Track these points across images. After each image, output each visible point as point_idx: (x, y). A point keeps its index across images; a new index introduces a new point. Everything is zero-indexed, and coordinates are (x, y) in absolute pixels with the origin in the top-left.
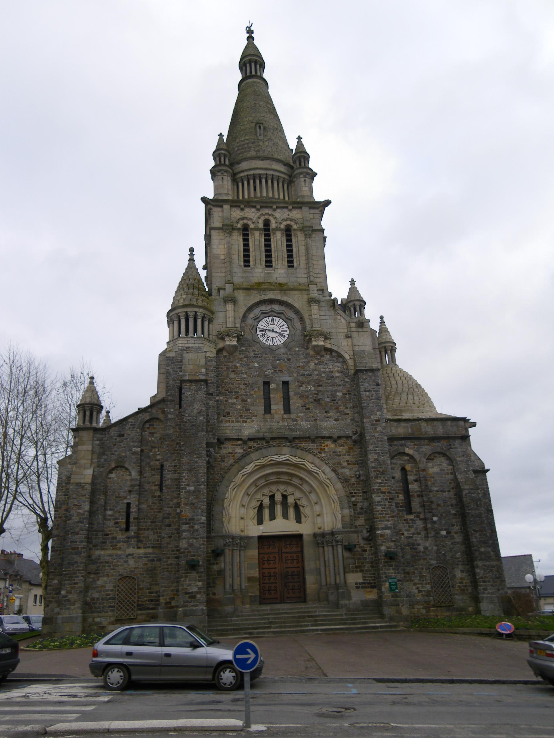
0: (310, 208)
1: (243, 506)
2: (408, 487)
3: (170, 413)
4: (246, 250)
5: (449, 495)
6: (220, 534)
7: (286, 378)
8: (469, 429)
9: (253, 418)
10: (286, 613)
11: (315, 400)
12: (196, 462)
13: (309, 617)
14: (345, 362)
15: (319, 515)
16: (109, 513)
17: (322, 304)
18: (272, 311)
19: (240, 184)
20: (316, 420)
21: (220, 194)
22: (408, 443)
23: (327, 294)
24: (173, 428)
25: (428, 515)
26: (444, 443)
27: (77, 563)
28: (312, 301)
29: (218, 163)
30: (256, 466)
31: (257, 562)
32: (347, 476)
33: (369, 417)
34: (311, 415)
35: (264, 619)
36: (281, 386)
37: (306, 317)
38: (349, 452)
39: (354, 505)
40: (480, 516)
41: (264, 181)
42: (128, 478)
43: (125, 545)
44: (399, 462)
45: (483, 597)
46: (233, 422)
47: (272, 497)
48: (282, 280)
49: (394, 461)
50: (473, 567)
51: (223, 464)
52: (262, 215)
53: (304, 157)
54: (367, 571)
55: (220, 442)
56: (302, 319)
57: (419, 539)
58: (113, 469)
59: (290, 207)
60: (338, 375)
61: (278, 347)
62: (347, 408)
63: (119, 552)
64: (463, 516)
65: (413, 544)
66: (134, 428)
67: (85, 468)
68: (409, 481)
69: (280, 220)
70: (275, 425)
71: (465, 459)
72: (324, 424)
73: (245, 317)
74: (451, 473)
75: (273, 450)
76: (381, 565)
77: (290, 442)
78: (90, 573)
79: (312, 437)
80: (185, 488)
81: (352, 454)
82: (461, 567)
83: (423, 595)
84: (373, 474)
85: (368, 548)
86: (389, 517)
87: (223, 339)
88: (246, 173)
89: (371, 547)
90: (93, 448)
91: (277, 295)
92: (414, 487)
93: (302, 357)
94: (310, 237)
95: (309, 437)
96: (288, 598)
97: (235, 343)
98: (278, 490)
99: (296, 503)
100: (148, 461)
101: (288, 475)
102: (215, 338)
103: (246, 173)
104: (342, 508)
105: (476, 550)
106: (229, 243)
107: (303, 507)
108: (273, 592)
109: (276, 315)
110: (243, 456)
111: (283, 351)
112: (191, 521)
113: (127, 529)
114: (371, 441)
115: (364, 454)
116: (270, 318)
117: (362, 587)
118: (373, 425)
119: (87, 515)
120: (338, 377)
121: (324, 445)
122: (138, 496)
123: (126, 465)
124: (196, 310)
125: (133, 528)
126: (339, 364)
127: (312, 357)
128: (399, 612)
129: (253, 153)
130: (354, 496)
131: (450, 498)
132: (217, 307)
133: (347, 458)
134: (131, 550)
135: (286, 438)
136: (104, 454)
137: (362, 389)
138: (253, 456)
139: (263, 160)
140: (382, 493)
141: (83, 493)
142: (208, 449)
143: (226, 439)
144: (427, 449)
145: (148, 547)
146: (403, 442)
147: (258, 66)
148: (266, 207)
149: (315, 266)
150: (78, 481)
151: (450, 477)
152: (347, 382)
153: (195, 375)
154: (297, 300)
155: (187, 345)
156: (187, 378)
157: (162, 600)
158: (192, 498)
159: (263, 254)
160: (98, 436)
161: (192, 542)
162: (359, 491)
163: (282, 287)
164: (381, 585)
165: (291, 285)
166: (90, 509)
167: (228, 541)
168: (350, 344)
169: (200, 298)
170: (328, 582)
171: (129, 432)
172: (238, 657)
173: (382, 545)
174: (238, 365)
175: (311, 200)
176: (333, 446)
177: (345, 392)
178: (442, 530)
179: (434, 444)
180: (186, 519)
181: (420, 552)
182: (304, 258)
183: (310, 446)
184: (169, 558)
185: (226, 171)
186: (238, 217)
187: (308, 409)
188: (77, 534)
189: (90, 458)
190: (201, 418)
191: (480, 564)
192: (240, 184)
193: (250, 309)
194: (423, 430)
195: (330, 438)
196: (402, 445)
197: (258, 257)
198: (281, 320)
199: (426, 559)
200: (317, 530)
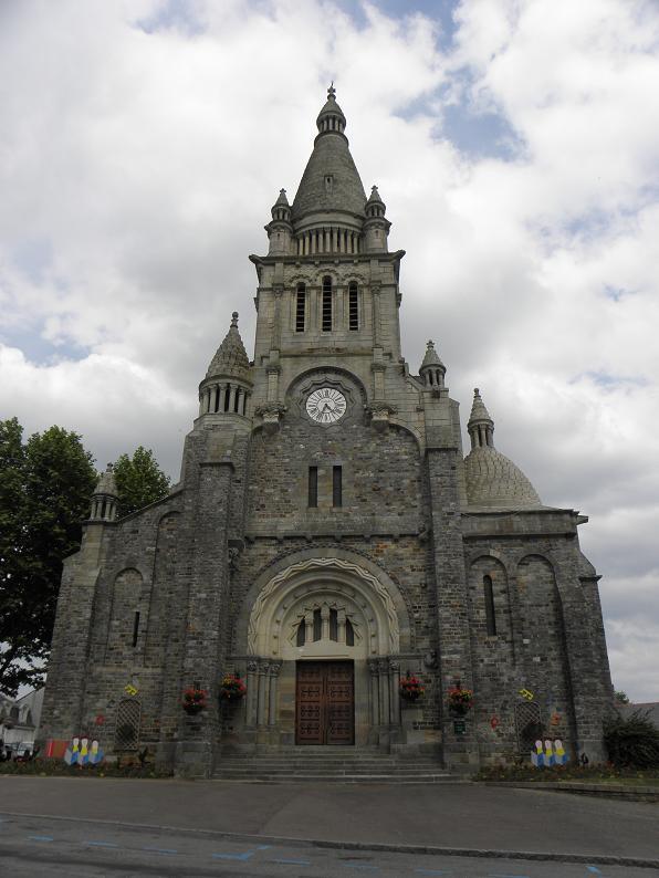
0: (380, 261)
1: (278, 622)
4: (301, 312)
5: (547, 611)
10: (320, 757)
11: (374, 490)
14: (415, 441)
15: (373, 636)
16: (116, 623)
17: (388, 371)
19: (301, 242)
20: (373, 514)
22: (495, 543)
25: (517, 636)
26: (543, 543)
27: (72, 679)
31: (294, 692)
33: (440, 509)
34: (368, 508)
35: (290, 762)
42: (140, 582)
44: (480, 570)
45: (583, 743)
46: (268, 516)
47: (317, 613)
48: (341, 345)
52: (322, 271)
53: (378, 207)
54: (429, 707)
55: (250, 541)
56: (363, 390)
57: (502, 667)
58: (123, 571)
61: (332, 425)
63: (123, 671)
64: (562, 636)
65: (494, 674)
67: (91, 569)
68: (495, 593)
70: (320, 520)
73: (291, 389)
74: (551, 582)
75: (316, 551)
80: (195, 595)
82: (557, 704)
83: (503, 740)
84: (440, 583)
88: (307, 229)
90: (102, 545)
92: (499, 600)
94: (378, 292)
96: (332, 739)
97: (276, 420)
99: (348, 620)
103: (307, 229)
104: (401, 627)
105: (578, 682)
110: (277, 559)
111: (336, 429)
112: (199, 636)
113: (134, 645)
114: (441, 539)
115: (431, 558)
118: (444, 519)
119: (87, 623)
122: (148, 605)
123: (138, 568)
125: (140, 642)
127: (373, 436)
129: (318, 207)
133: (412, 562)
134: (136, 669)
137: (432, 473)
138: (289, 559)
141: (85, 598)
143: (257, 538)
144: (519, 550)
146: (488, 542)
148: (326, 263)
149: (383, 327)
150: (80, 583)
153: (218, 457)
154: (358, 367)
155: (214, 423)
156: (208, 460)
161: (202, 664)
162: (426, 601)
163: (340, 353)
174: (279, 447)
176: (393, 547)
177: (413, 478)
179: (529, 544)
185: (283, 228)
187: (365, 500)
191: (581, 699)
192: (301, 242)
193: (299, 379)
194: (515, 527)
195: (389, 536)
196: (486, 546)
200: (371, 656)
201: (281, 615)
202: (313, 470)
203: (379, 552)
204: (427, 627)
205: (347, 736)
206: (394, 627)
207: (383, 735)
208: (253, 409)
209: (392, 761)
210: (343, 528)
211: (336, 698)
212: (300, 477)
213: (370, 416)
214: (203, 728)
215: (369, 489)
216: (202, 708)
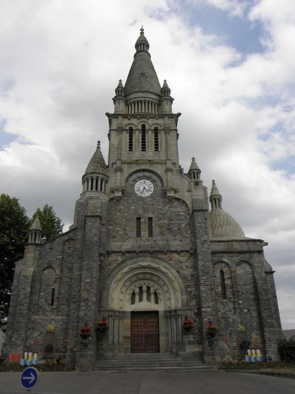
0: (169, 118)
1: (122, 293)
2: (224, 282)
3: (79, 235)
5: (250, 287)
7: (151, 215)
8: (264, 247)
12: (92, 265)
13: (159, 361)
14: (187, 206)
17: (174, 172)
18: (144, 176)
19: (130, 107)
21: (118, 111)
22: (225, 255)
23: (177, 166)
25: (236, 300)
29: (118, 94)
31: (130, 327)
36: (147, 220)
37: (164, 180)
40: (268, 300)
41: (143, 104)
42: (54, 274)
43: (51, 313)
47: (141, 288)
49: (216, 266)
50: (263, 332)
51: (110, 266)
53: (167, 90)
55: (109, 253)
56: (162, 180)
57: (230, 314)
58: (46, 268)
59: (157, 117)
60: (183, 213)
61: (147, 197)
62: (187, 234)
64: (257, 300)
67: (30, 267)
68: (225, 278)
69: (151, 125)
70: (142, 244)
71: (260, 265)
72: (173, 243)
74: (252, 274)
75: (140, 258)
78: (29, 329)
82: (256, 332)
83: (231, 349)
84: (201, 274)
87: (113, 192)
88: (133, 100)
90: (35, 255)
91: (147, 167)
92: (228, 282)
94: (168, 133)
95: (163, 251)
99: (155, 292)
101: (151, 274)
102: (109, 192)
103: (133, 100)
104: (182, 295)
105: (264, 321)
106: (120, 137)
108: (139, 346)
110: (122, 262)
113: (52, 304)
114: (201, 253)
117: (193, 344)
119: (29, 294)
120: (183, 215)
124: (98, 175)
125: (55, 304)
128: (214, 360)
129: (138, 89)
131: (250, 289)
132: (111, 174)
133: (187, 264)
134: (53, 317)
135: (149, 252)
136: (41, 259)
137: (196, 222)
138: (129, 262)
139: (143, 93)
140: (206, 285)
141: (28, 281)
144: (236, 258)
145: (64, 315)
146: (222, 254)
147: (145, 47)
148: (143, 118)
151: (251, 276)
154: (159, 169)
155: (91, 196)
156: (89, 214)
157: (68, 347)
158: (88, 286)
159: (141, 144)
160: (38, 248)
161: (88, 315)
163: (150, 162)
165: (155, 161)
166: (31, 291)
169: (101, 169)
171: (56, 247)
172: (24, 378)
174: (122, 208)
175: (170, 113)
176: (178, 256)
178: (244, 309)
180: (84, 299)
181: (230, 322)
182: (164, 145)
183: (163, 256)
184: (73, 322)
185: (121, 99)
186: (127, 123)
187: (163, 234)
188: (23, 305)
189: (33, 261)
191: (267, 330)
192: (130, 107)
193: (131, 175)
195: (176, 252)
196: (221, 256)
197: (137, 145)
198: (149, 182)
199: (233, 327)
200: (167, 309)
202: (139, 219)
203: (171, 259)
206: (179, 294)
207: (174, 347)
209: (179, 360)
212: (132, 222)
214: (89, 346)
215: (165, 229)
216: (89, 336)
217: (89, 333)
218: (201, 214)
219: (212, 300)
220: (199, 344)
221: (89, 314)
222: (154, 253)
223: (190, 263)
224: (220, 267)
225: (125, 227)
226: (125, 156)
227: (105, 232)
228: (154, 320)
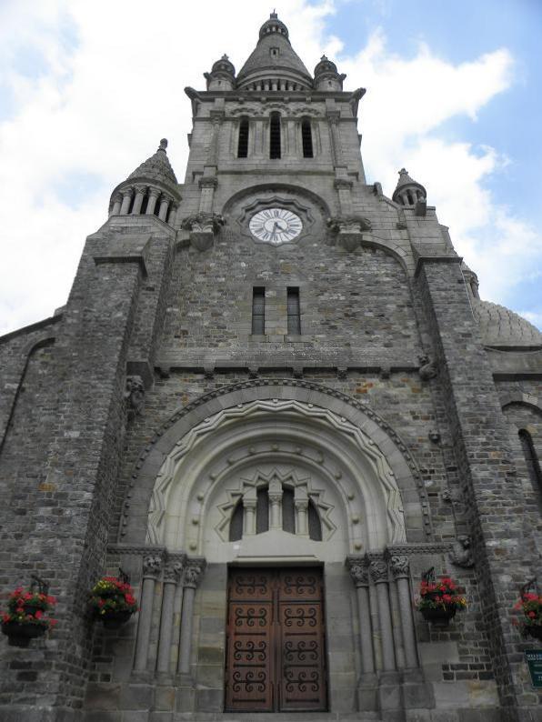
1: (200, 499)
6: (137, 546)
7: (295, 282)
9: (230, 341)
11: (347, 315)
12: (94, 387)
14: (397, 260)
15: (356, 522)
18: (276, 201)
22: (527, 385)
24: (72, 339)
28: (338, 185)
30: (228, 418)
31: (223, 615)
32: (414, 440)
33: (450, 330)
38: (413, 396)
39: (430, 495)
46: (191, 345)
47: (263, 491)
51: (161, 412)
54: (467, 637)
55: (162, 374)
60: (388, 279)
62: (406, 328)
66: (16, 353)
70: (269, 350)
73: (229, 206)
75: (265, 391)
76: (504, 620)
77: (297, 377)
79: (340, 369)
81: (421, 400)
84: (467, 427)
85: (468, 587)
86: (510, 512)
89: (474, 583)
93: (323, 255)
96: (288, 701)
97: (210, 231)
98: (275, 476)
99: (311, 504)
100: (30, 407)
104: (405, 501)
107: (325, 509)
108: (255, 686)
109: (282, 206)
110: (204, 400)
114: (459, 368)
116: (272, 210)
117: (460, 677)
120: (388, 282)
121: (364, 384)
126: (389, 265)
127: (342, 255)
130: (429, 478)
135: (289, 370)
137: (432, 287)
138: (224, 401)
140: (491, 462)
142: (130, 377)
146: (517, 384)
152: (404, 289)
154: (318, 186)
164: (509, 669)
167: (152, 561)
168: (405, 237)
170: (379, 665)
173: (501, 572)
174: (212, 265)
176: (381, 385)
177: (401, 303)
180: (49, 495)
183: (336, 385)
185: (225, 76)
187: (334, 327)
190: (120, 314)
193: (240, 196)
195: (375, 371)
196: (515, 389)
198: (290, 213)
201: (206, 489)
202: (259, 292)
203: (362, 393)
204: (448, 501)
205: (314, 695)
206: (394, 501)
207: (389, 691)
208: (179, 222)
210: (306, 358)
211: (295, 629)
212: (240, 298)
213: (337, 230)
214: (42, 675)
216: (41, 629)
217: (43, 617)
218: (445, 270)
219: (519, 511)
220: (484, 677)
221: (61, 551)
222: (306, 374)
223: (423, 404)
224: (515, 419)
225: (218, 310)
226: (229, 163)
227: (151, 307)
228: (306, 596)
